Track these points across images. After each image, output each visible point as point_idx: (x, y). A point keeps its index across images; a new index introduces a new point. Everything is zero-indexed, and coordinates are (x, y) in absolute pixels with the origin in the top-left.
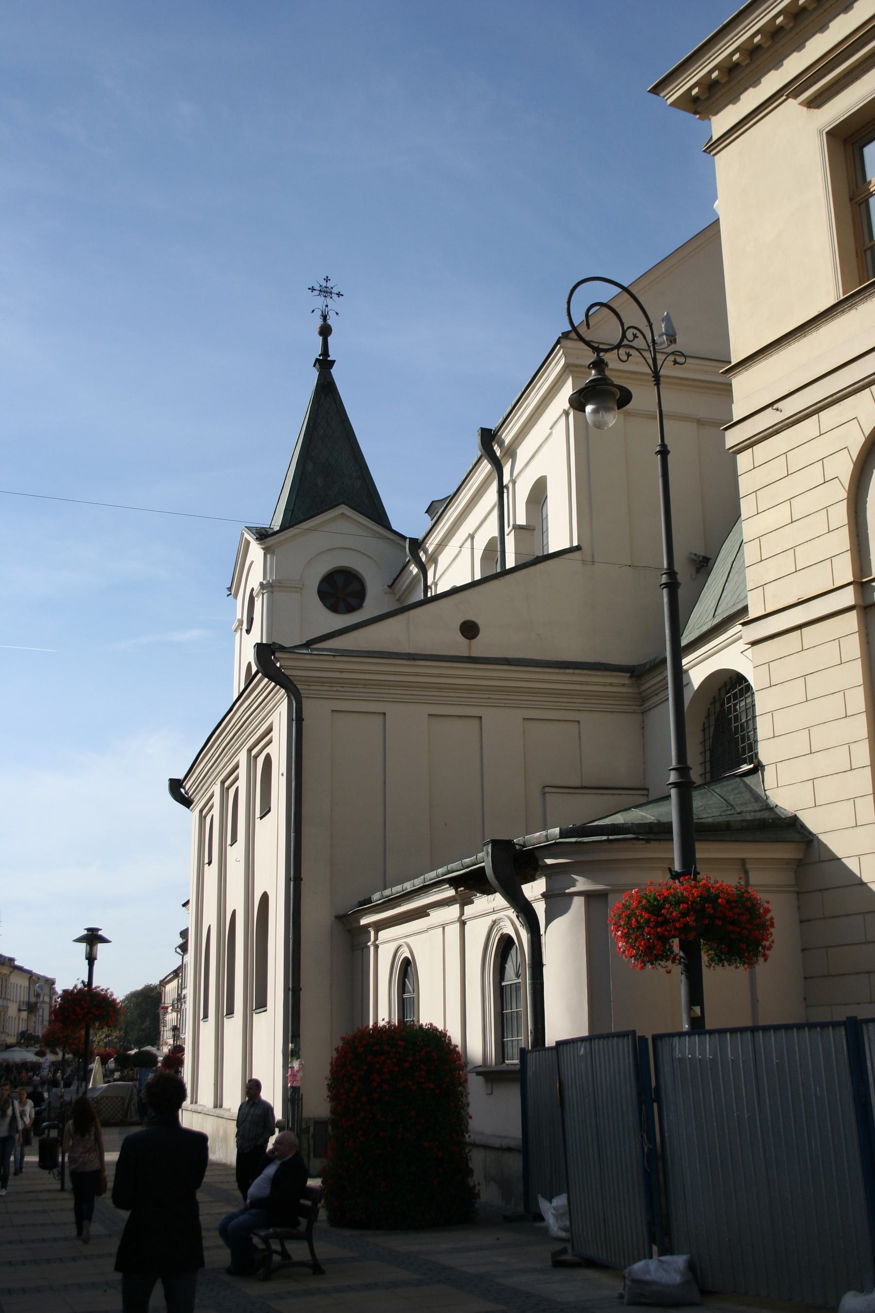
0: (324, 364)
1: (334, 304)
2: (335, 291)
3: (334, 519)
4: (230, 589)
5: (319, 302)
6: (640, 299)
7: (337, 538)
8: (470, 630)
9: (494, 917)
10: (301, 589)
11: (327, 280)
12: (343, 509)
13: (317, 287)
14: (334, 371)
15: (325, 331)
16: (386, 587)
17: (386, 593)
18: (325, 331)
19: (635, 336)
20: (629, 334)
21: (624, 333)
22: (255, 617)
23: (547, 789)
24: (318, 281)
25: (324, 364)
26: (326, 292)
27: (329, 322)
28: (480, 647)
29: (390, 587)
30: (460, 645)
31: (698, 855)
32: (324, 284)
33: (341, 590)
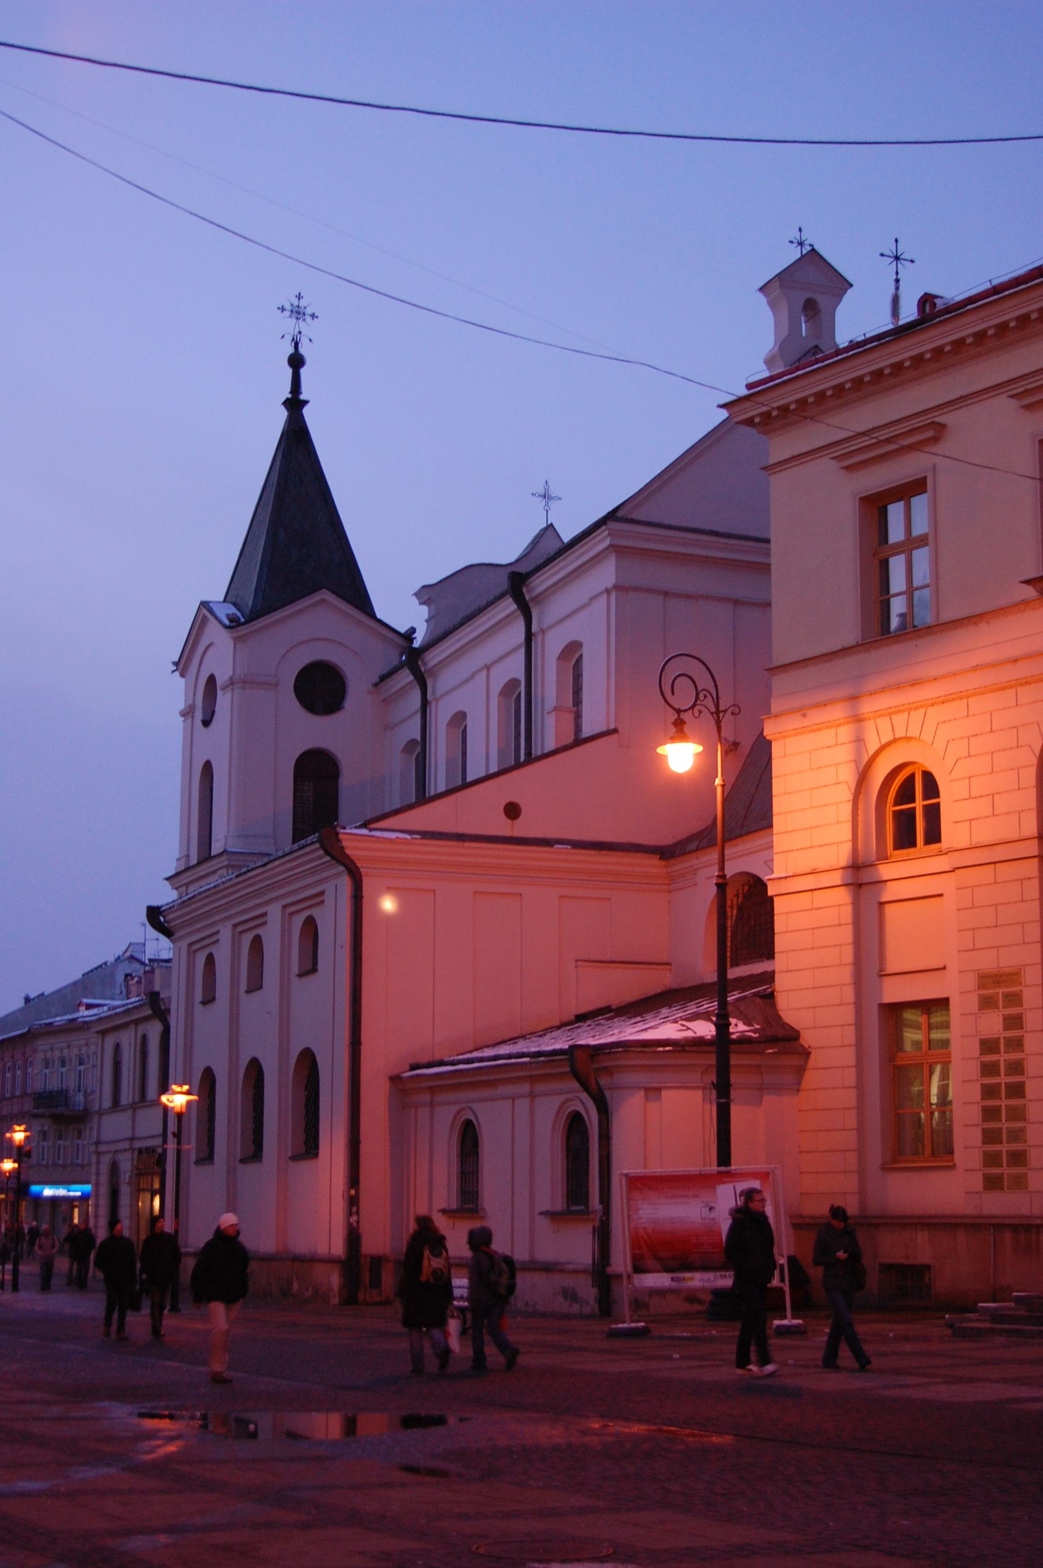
0: (295, 404)
1: (308, 328)
2: (308, 311)
3: (314, 604)
4: (176, 664)
5: (290, 326)
6: (710, 667)
7: (312, 628)
8: (512, 811)
9: (568, 1096)
10: (276, 685)
11: (299, 297)
12: (325, 595)
13: (288, 307)
14: (306, 411)
15: (296, 362)
16: (370, 685)
17: (369, 692)
18: (296, 362)
19: (705, 697)
20: (701, 696)
21: (697, 694)
22: (218, 708)
23: (579, 963)
24: (288, 299)
25: (295, 404)
26: (298, 313)
27: (302, 350)
28: (521, 828)
29: (376, 685)
30: (504, 827)
31: (732, 1062)
32: (295, 302)
33: (320, 688)
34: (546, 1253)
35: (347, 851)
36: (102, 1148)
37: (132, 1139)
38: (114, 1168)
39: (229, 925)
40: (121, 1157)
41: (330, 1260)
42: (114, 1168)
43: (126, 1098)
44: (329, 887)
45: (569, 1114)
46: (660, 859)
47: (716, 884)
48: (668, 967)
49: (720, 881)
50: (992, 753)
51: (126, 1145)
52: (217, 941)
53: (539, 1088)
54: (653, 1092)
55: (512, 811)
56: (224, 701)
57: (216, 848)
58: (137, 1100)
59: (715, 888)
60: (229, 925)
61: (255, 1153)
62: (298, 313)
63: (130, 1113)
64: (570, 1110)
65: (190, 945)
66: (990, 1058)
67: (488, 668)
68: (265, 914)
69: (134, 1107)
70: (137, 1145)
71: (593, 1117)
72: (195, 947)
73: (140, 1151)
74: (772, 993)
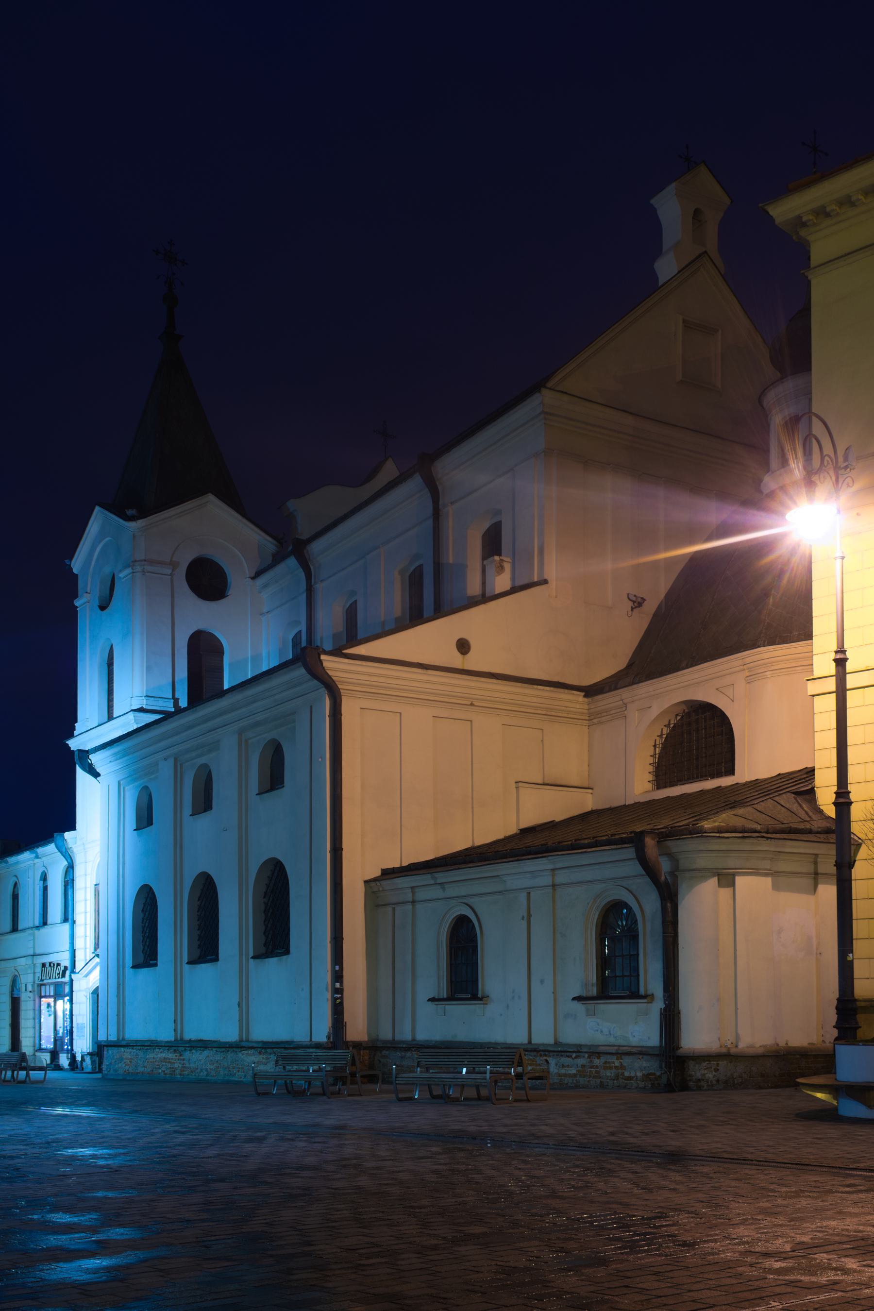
8: (463, 646)
23: (520, 784)
28: (472, 662)
30: (456, 660)
34: (572, 1035)
35: (329, 672)
41: (642, 1052)
45: (609, 902)
46: (585, 696)
47: (835, 660)
48: (590, 791)
49: (839, 656)
54: (727, 879)
55: (463, 646)
59: (834, 664)
61: (205, 948)
64: (459, 913)
66: (47, 965)
71: (648, 905)
74: (813, 788)
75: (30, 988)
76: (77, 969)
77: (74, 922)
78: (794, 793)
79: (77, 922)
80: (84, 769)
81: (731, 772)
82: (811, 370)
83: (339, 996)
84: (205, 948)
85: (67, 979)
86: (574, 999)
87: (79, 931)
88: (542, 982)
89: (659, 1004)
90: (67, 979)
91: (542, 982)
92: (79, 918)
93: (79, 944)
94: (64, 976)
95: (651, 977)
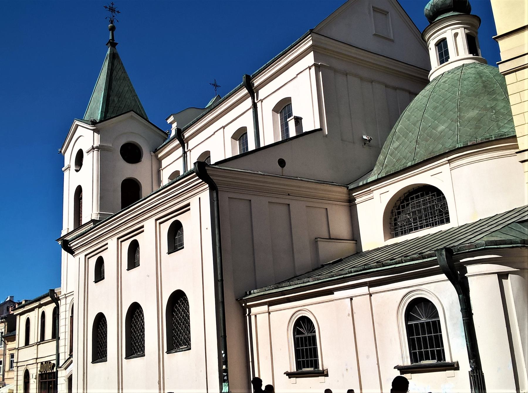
2: (116, 10)
8: (282, 163)
26: (112, 10)
36: (19, 364)
37: (37, 359)
38: (27, 374)
39: (153, 220)
40: (29, 367)
42: (27, 374)
43: (32, 341)
44: (194, 202)
50: (351, 299)
51: (34, 361)
52: (107, 248)
53: (272, 308)
55: (282, 163)
56: (87, 159)
57: (85, 219)
58: (39, 341)
60: (153, 220)
61: (135, 347)
62: (112, 10)
63: (36, 347)
64: (301, 315)
65: (86, 255)
66: (44, 363)
67: (224, 127)
68: (188, 205)
69: (38, 344)
70: (39, 361)
72: (88, 257)
73: (42, 363)
75: (34, 377)
76: (60, 365)
77: (59, 338)
78: (519, 222)
79: (61, 338)
80: (65, 250)
81: (448, 221)
82: (106, 356)
83: (225, 374)
84: (135, 347)
85: (55, 370)
86: (395, 368)
87: (62, 342)
88: (368, 357)
89: (465, 366)
90: (55, 370)
91: (368, 357)
92: (62, 335)
93: (61, 350)
94: (53, 369)
95: (455, 347)
